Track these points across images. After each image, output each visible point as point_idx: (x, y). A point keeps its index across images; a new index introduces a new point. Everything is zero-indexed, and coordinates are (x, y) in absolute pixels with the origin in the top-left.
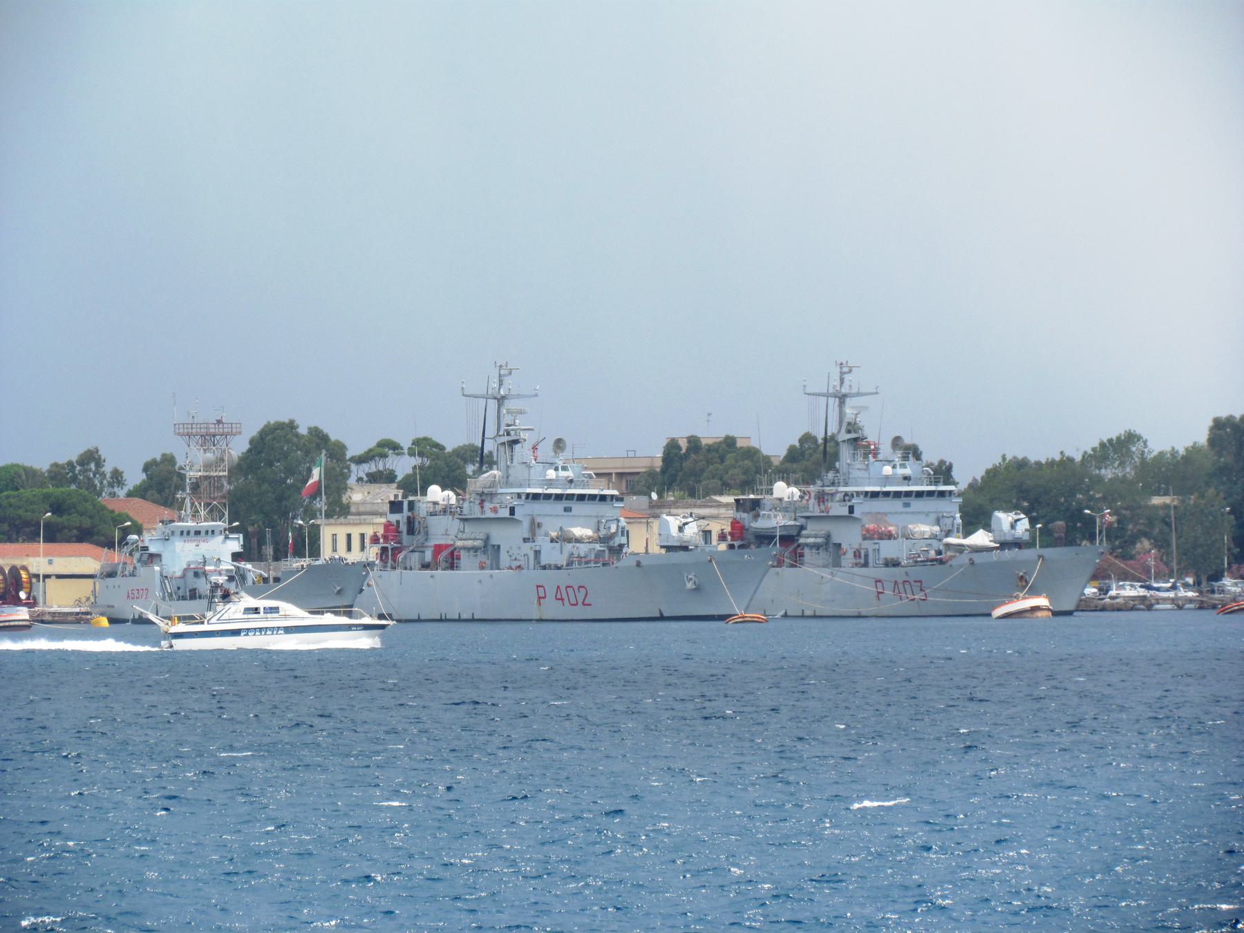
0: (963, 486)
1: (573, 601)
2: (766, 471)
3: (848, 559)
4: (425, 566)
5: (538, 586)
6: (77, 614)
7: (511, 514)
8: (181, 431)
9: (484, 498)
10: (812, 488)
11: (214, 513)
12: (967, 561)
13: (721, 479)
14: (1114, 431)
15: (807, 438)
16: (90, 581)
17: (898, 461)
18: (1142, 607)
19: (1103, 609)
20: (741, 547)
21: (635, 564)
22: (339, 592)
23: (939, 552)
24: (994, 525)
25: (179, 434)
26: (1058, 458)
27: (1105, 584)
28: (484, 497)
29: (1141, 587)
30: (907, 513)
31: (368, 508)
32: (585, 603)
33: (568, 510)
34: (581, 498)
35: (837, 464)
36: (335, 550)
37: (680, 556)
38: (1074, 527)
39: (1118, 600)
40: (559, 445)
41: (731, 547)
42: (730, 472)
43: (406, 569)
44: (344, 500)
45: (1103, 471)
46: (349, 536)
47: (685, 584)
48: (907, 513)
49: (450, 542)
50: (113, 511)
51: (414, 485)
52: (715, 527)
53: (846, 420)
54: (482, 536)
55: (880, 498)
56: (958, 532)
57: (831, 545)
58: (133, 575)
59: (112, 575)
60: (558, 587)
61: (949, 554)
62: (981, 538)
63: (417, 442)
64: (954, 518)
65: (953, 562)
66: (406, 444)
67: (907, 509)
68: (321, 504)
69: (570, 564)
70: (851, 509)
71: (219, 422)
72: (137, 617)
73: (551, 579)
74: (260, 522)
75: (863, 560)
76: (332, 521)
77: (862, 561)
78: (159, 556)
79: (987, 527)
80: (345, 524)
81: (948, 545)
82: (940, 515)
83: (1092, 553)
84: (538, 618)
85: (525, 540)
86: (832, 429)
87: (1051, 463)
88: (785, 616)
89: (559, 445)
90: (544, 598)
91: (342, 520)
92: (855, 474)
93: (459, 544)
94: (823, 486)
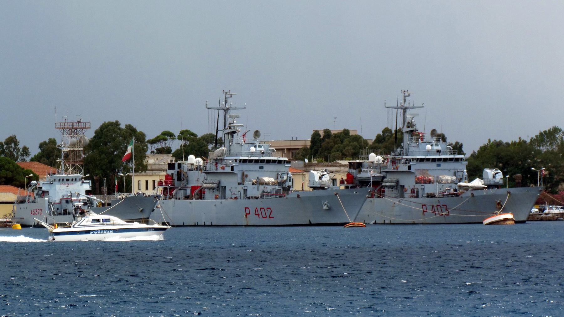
0: (468, 155)
1: (264, 216)
2: (365, 148)
3: (408, 194)
4: (187, 197)
5: (246, 208)
6: (5, 222)
7: (231, 170)
8: (59, 126)
9: (217, 162)
10: (389, 157)
11: (76, 170)
12: (470, 195)
13: (341, 152)
14: (547, 127)
15: (386, 130)
16: (12, 205)
17: (434, 142)
18: (562, 218)
19: (542, 220)
20: (351, 187)
21: (296, 196)
22: (142, 211)
23: (455, 190)
24: (484, 176)
25: (58, 128)
26: (518, 141)
27: (542, 206)
28: (217, 161)
29: (561, 208)
30: (439, 169)
31: (157, 167)
32: (271, 216)
33: (261, 168)
34: (268, 162)
35: (402, 144)
36: (139, 189)
37: (320, 192)
38: (527, 177)
39: (549, 215)
40: (257, 134)
41: (347, 187)
42: (346, 148)
43: (176, 199)
44: (144, 163)
45: (541, 148)
46: (147, 182)
47: (323, 207)
48: (439, 169)
49: (200, 185)
50: (23, 169)
51: (181, 155)
52: (339, 177)
53: (407, 121)
54: (217, 182)
55: (425, 162)
56: (465, 179)
57: (399, 186)
58: (34, 202)
59: (23, 202)
60: (256, 208)
61: (461, 191)
62: (477, 183)
63: (182, 133)
64: (463, 172)
65: (463, 195)
66: (177, 133)
67: (439, 168)
68: (132, 165)
69: (262, 196)
70: (410, 168)
71: (79, 122)
72: (36, 224)
73: (253, 204)
74: (101, 174)
75: (415, 194)
76: (138, 174)
77: (415, 195)
78: (47, 192)
79: (481, 177)
80: (145, 175)
81: (460, 187)
82: (456, 171)
83: (536, 190)
84: (246, 224)
85: (239, 184)
86: (400, 126)
87: (514, 144)
88: (375, 223)
89: (257, 134)
90: (249, 214)
91: (143, 173)
92: (412, 149)
93: (204, 186)
94: (395, 155)
